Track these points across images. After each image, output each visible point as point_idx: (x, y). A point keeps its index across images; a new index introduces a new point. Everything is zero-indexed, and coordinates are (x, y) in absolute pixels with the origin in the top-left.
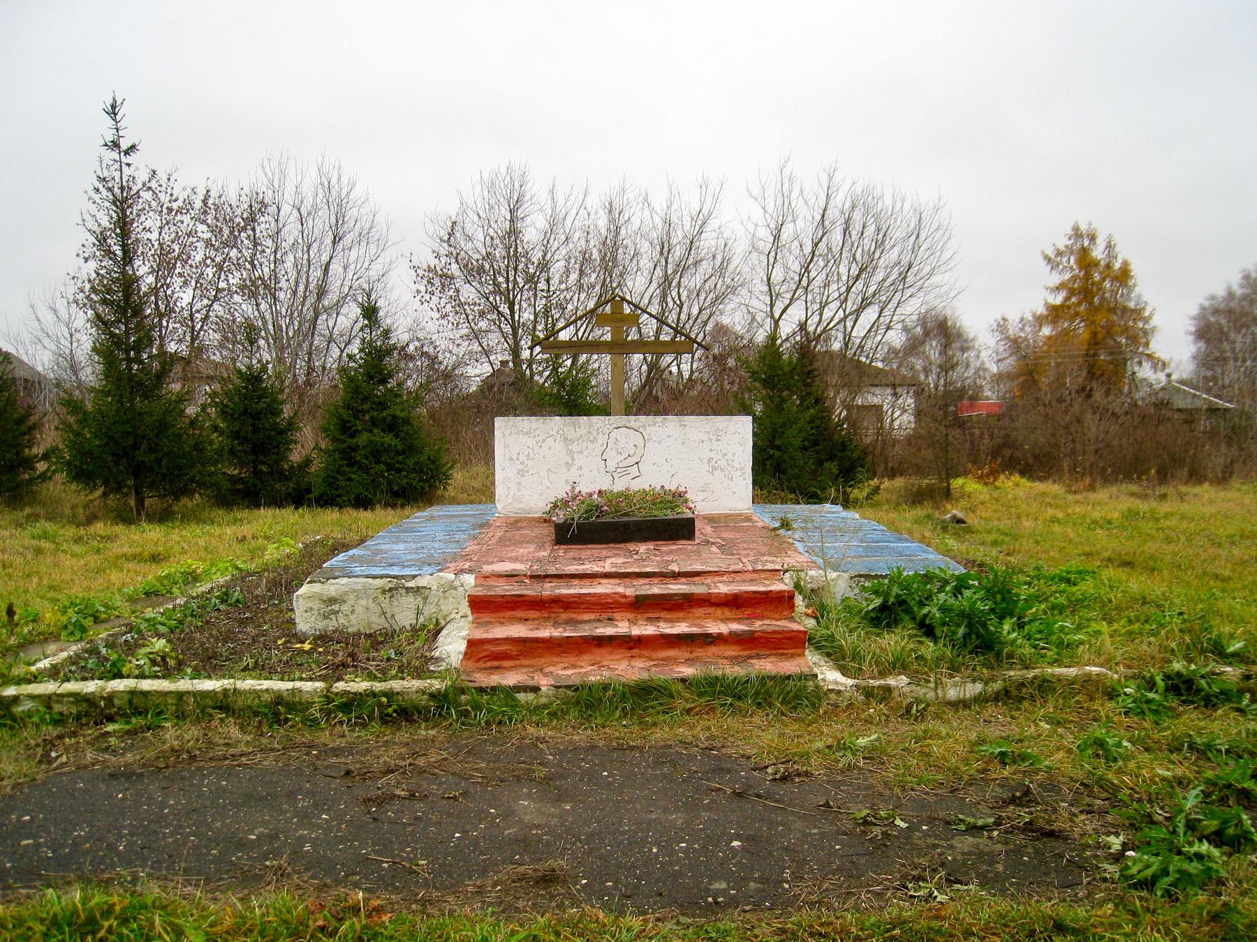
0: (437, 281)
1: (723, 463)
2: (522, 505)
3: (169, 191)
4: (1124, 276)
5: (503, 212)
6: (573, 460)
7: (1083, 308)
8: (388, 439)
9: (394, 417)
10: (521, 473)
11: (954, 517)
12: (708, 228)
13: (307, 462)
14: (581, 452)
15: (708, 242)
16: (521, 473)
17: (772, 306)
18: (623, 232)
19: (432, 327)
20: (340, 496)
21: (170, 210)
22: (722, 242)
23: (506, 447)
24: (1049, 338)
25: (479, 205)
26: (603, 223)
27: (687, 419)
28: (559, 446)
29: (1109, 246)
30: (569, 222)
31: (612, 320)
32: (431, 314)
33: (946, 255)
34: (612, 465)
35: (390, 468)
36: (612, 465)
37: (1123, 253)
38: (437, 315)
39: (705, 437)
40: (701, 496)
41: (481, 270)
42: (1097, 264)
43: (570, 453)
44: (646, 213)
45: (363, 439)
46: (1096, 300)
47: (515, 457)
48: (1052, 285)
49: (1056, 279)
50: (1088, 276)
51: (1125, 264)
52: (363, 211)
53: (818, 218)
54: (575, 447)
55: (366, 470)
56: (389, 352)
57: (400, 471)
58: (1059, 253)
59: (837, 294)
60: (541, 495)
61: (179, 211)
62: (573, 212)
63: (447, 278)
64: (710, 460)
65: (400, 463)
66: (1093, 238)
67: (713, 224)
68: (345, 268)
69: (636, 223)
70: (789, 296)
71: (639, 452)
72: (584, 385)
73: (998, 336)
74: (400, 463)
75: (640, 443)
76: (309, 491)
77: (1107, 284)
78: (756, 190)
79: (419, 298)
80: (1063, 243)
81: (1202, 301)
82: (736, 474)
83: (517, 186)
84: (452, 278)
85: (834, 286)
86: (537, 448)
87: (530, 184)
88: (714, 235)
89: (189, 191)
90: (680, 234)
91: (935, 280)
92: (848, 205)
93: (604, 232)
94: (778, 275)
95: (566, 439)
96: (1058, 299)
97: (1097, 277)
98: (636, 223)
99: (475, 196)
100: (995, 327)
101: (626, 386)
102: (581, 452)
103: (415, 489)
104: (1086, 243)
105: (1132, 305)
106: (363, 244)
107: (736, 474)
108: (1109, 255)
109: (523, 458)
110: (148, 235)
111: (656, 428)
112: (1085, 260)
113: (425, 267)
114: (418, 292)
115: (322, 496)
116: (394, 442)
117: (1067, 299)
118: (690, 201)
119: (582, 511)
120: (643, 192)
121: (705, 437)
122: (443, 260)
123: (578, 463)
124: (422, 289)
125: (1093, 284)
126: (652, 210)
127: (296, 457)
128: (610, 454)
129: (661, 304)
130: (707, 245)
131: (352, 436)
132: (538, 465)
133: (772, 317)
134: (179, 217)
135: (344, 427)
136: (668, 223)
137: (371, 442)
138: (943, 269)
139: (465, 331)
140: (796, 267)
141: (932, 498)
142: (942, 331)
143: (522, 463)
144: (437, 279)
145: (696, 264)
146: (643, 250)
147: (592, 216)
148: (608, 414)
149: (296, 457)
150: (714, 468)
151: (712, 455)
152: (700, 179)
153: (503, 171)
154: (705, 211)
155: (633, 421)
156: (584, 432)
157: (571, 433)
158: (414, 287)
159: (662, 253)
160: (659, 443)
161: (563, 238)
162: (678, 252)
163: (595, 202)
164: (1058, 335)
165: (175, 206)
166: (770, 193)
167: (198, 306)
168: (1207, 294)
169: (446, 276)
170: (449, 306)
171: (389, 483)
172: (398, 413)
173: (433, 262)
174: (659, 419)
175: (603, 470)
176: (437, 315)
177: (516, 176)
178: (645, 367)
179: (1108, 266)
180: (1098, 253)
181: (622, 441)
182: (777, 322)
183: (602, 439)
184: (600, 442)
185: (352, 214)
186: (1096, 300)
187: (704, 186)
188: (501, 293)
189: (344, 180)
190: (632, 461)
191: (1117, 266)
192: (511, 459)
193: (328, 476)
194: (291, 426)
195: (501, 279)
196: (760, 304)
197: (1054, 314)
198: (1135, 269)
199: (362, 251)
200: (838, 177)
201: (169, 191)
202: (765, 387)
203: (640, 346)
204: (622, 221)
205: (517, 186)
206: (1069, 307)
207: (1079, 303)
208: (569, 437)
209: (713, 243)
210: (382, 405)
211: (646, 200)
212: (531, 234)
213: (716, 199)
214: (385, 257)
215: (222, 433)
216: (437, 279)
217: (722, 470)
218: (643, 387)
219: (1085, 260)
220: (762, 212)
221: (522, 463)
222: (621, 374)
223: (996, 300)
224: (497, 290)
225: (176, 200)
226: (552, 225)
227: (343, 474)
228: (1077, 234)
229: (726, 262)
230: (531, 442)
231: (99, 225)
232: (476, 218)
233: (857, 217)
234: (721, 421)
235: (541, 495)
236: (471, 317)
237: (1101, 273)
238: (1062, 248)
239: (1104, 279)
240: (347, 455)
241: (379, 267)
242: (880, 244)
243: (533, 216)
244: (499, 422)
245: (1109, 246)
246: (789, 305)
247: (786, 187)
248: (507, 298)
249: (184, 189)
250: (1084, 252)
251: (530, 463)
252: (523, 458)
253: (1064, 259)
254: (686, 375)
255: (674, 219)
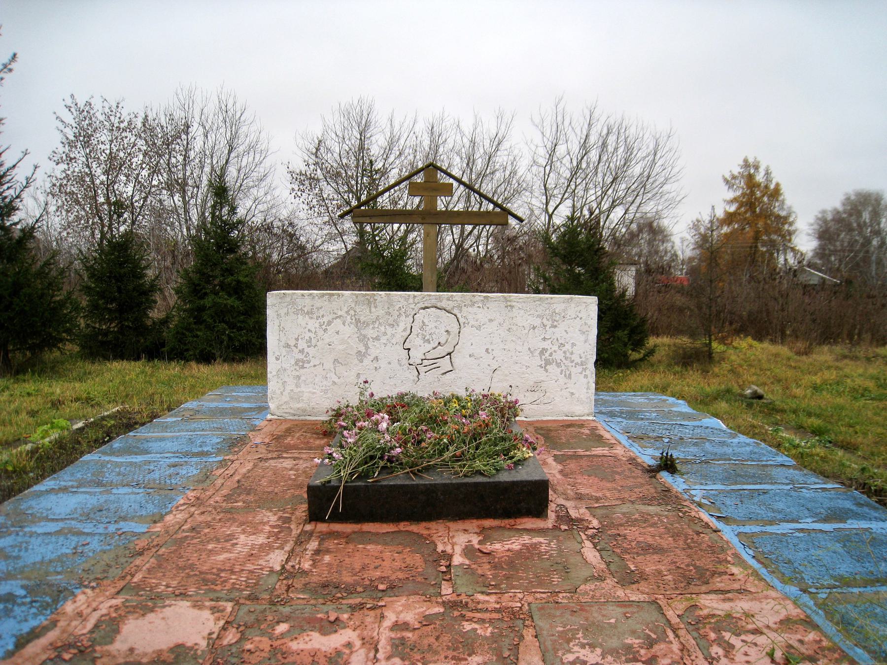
0: (307, 182)
1: (559, 356)
2: (300, 405)
3: (118, 115)
4: (776, 193)
5: (354, 132)
6: (367, 347)
7: (748, 215)
8: (232, 301)
9: (239, 282)
10: (300, 364)
11: (755, 392)
12: (502, 148)
13: (165, 322)
14: (377, 338)
15: (501, 158)
16: (300, 364)
17: (547, 204)
18: (441, 150)
19: (302, 215)
20: (187, 350)
21: (118, 128)
22: (511, 158)
23: (281, 329)
24: (726, 234)
25: (337, 127)
26: (426, 143)
27: (515, 297)
28: (348, 331)
29: (767, 173)
30: (402, 141)
31: (425, 189)
32: (302, 206)
33: (676, 170)
34: (417, 355)
35: (232, 326)
36: (417, 355)
37: (777, 177)
38: (307, 207)
39: (537, 322)
40: (531, 397)
41: (338, 174)
42: (758, 185)
43: (363, 339)
44: (458, 137)
45: (208, 302)
46: (757, 208)
47: (292, 343)
48: (728, 199)
49: (731, 195)
50: (752, 193)
51: (777, 185)
52: (252, 129)
53: (582, 141)
54: (370, 332)
55: (210, 328)
56: (234, 226)
57: (241, 329)
58: (734, 177)
59: (593, 198)
60: (325, 392)
61: (124, 130)
62: (405, 136)
63: (313, 180)
64: (543, 351)
65: (243, 322)
66: (757, 168)
67: (505, 145)
68: (239, 171)
69: (450, 144)
70: (560, 196)
71: (452, 340)
72: (402, 257)
73: (693, 232)
74: (243, 322)
75: (454, 328)
76: (163, 345)
77: (765, 199)
78: (537, 120)
79: (293, 194)
80: (737, 170)
81: (817, 214)
82: (575, 371)
83: (365, 114)
84: (318, 180)
85: (592, 192)
86: (320, 333)
87: (375, 113)
88: (506, 153)
89: (132, 116)
90: (482, 151)
91: (666, 187)
92: (605, 131)
93: (427, 149)
94: (551, 183)
95: (358, 321)
96: (732, 208)
97: (758, 194)
98: (450, 144)
99: (335, 122)
100: (691, 226)
101: (440, 260)
102: (377, 338)
103: (254, 344)
104: (752, 171)
105: (783, 214)
106: (252, 153)
107: (575, 371)
108: (767, 180)
109: (302, 344)
110: (103, 147)
111: (474, 309)
112: (751, 182)
113: (298, 172)
114: (293, 189)
115: (172, 350)
116: (237, 303)
117: (738, 208)
118: (490, 127)
119: (358, 458)
120: (456, 121)
121: (537, 322)
122: (312, 167)
123: (374, 352)
124: (296, 188)
125: (756, 198)
126: (461, 132)
127: (155, 314)
128: (415, 342)
129: (466, 202)
130: (501, 160)
131: (202, 298)
132: (326, 355)
133: (547, 211)
134: (124, 134)
135: (195, 289)
136: (473, 142)
137: (215, 304)
138: (672, 180)
139: (326, 219)
140: (568, 174)
141: (698, 360)
142: (652, 230)
143: (302, 351)
144: (305, 181)
145: (493, 173)
146: (455, 163)
147: (419, 139)
148: (419, 289)
149: (155, 314)
150: (548, 362)
151: (546, 345)
152: (497, 112)
153: (356, 103)
154: (500, 135)
155: (447, 298)
156: (381, 312)
157: (364, 314)
158: (291, 186)
159: (468, 164)
160: (479, 328)
161: (398, 153)
162: (479, 164)
163: (421, 128)
164: (731, 233)
165: (122, 126)
166: (547, 124)
167: (137, 198)
168: (820, 209)
169: (314, 179)
170: (314, 200)
171: (230, 339)
172: (241, 279)
173: (304, 168)
174: (479, 296)
175: (405, 362)
176: (307, 207)
177: (365, 108)
178: (454, 247)
179: (766, 187)
180: (760, 178)
181: (431, 325)
182: (550, 217)
183: (404, 323)
184: (402, 325)
185: (243, 130)
186: (757, 208)
187: (500, 117)
188: (353, 192)
189: (238, 106)
190: (441, 351)
191: (772, 187)
192: (288, 346)
193: (178, 333)
194: (153, 288)
195: (353, 182)
196: (538, 202)
197: (730, 218)
198: (784, 189)
199: (251, 159)
200: (596, 115)
201: (118, 115)
202: (564, 262)
203: (452, 218)
204: (441, 141)
205: (365, 114)
206: (739, 214)
207: (745, 212)
208: (362, 319)
209: (505, 159)
210: (229, 271)
211: (458, 126)
212: (375, 149)
213: (508, 127)
214: (267, 163)
215: (842, 245)
216: (305, 181)
217: (558, 365)
218: (453, 260)
219: (751, 182)
220: (541, 135)
221: (302, 351)
222: (433, 245)
223: (689, 211)
224: (350, 191)
225: (122, 122)
226: (391, 143)
227: (190, 330)
228: (746, 164)
229: (514, 173)
230: (313, 324)
231: (67, 139)
232: (334, 136)
233: (612, 139)
234: (559, 300)
235: (325, 392)
236: (330, 209)
237: (761, 192)
238: (736, 173)
239: (763, 196)
240: (197, 314)
241: (262, 170)
242: (627, 161)
243: (377, 137)
244: (273, 298)
245: (767, 173)
246: (560, 203)
247: (560, 118)
248: (357, 195)
249: (129, 114)
250: (750, 177)
251: (311, 351)
252: (302, 344)
253: (737, 182)
254: (483, 254)
255: (477, 140)
